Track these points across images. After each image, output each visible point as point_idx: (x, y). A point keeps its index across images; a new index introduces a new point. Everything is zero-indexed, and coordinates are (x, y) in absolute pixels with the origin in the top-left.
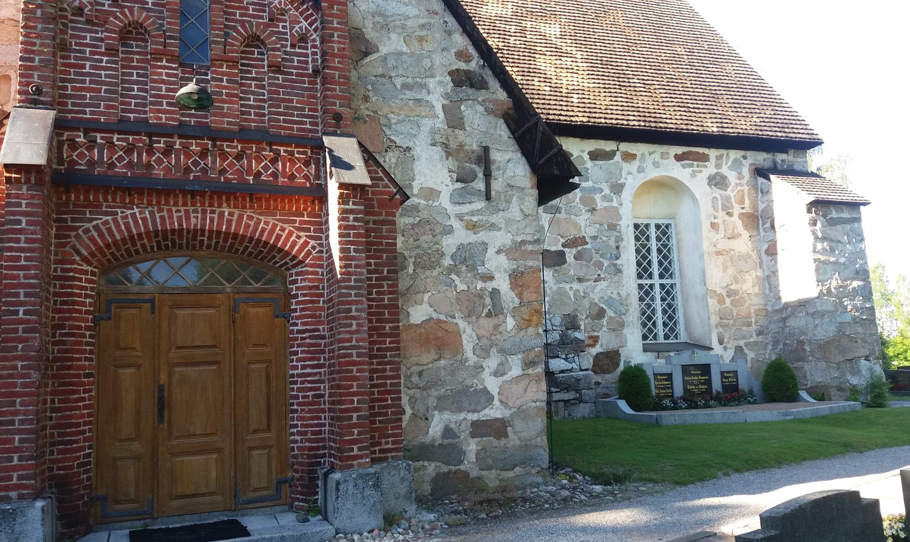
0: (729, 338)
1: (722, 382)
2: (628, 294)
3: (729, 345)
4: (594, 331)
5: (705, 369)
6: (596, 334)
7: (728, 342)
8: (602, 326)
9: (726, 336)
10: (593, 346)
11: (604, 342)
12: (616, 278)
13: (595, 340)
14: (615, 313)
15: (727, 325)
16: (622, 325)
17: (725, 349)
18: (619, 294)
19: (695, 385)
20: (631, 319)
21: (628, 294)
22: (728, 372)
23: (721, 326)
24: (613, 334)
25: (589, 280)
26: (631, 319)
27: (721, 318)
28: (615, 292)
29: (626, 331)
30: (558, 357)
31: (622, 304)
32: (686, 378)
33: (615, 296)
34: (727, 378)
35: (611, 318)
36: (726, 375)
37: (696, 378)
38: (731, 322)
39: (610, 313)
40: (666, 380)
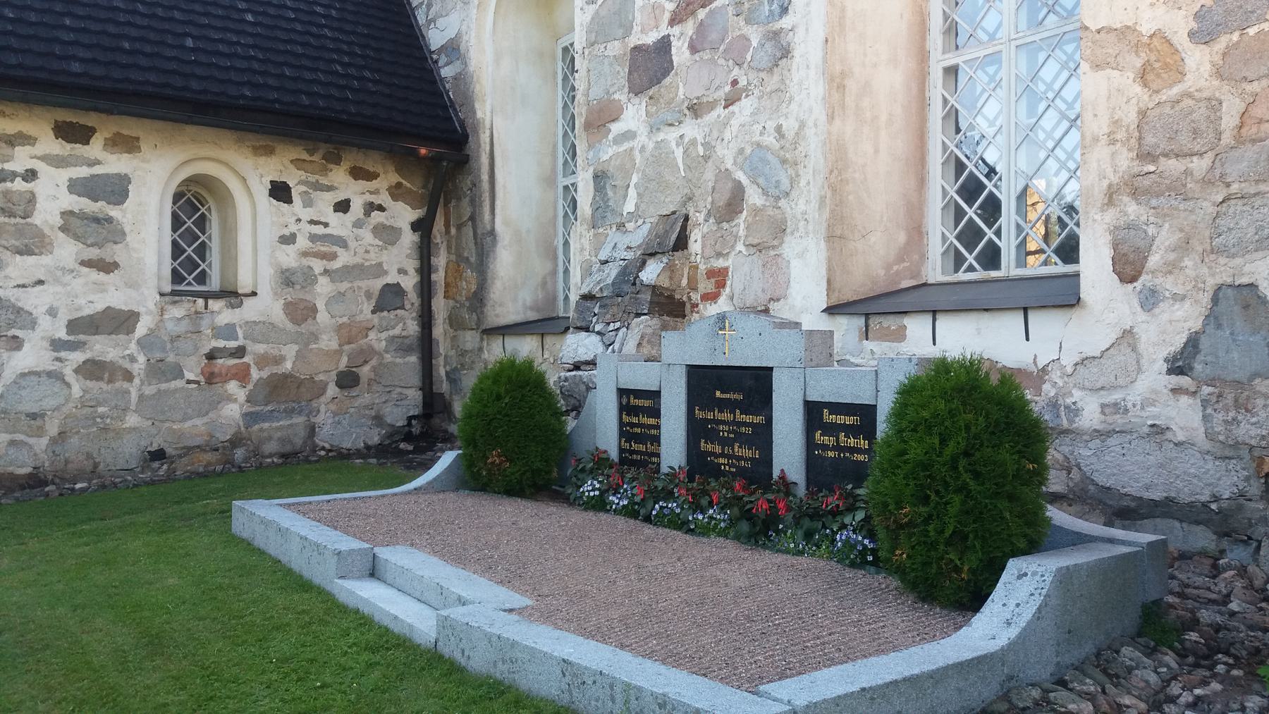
0: (1184, 246)
1: (810, 444)
2: (802, 125)
3: (1169, 284)
4: (719, 255)
5: (754, 385)
6: (720, 263)
7: (1171, 268)
8: (736, 237)
9: (1165, 237)
10: (712, 297)
11: (738, 287)
12: (773, 82)
13: (719, 277)
14: (765, 193)
15: (1177, 189)
16: (780, 230)
17: (1150, 300)
18: (779, 129)
19: (724, 442)
20: (801, 206)
21: (802, 125)
22: (836, 408)
23: (1135, 193)
24: (757, 260)
25: (712, 106)
26: (801, 206)
27: (1146, 156)
28: (771, 125)
29: (791, 247)
30: (587, 329)
31: (784, 162)
32: (699, 414)
33: (770, 140)
34: (831, 429)
35: (756, 211)
36: (828, 417)
37: (726, 416)
38: (1200, 165)
39: (754, 197)
40: (851, 430)
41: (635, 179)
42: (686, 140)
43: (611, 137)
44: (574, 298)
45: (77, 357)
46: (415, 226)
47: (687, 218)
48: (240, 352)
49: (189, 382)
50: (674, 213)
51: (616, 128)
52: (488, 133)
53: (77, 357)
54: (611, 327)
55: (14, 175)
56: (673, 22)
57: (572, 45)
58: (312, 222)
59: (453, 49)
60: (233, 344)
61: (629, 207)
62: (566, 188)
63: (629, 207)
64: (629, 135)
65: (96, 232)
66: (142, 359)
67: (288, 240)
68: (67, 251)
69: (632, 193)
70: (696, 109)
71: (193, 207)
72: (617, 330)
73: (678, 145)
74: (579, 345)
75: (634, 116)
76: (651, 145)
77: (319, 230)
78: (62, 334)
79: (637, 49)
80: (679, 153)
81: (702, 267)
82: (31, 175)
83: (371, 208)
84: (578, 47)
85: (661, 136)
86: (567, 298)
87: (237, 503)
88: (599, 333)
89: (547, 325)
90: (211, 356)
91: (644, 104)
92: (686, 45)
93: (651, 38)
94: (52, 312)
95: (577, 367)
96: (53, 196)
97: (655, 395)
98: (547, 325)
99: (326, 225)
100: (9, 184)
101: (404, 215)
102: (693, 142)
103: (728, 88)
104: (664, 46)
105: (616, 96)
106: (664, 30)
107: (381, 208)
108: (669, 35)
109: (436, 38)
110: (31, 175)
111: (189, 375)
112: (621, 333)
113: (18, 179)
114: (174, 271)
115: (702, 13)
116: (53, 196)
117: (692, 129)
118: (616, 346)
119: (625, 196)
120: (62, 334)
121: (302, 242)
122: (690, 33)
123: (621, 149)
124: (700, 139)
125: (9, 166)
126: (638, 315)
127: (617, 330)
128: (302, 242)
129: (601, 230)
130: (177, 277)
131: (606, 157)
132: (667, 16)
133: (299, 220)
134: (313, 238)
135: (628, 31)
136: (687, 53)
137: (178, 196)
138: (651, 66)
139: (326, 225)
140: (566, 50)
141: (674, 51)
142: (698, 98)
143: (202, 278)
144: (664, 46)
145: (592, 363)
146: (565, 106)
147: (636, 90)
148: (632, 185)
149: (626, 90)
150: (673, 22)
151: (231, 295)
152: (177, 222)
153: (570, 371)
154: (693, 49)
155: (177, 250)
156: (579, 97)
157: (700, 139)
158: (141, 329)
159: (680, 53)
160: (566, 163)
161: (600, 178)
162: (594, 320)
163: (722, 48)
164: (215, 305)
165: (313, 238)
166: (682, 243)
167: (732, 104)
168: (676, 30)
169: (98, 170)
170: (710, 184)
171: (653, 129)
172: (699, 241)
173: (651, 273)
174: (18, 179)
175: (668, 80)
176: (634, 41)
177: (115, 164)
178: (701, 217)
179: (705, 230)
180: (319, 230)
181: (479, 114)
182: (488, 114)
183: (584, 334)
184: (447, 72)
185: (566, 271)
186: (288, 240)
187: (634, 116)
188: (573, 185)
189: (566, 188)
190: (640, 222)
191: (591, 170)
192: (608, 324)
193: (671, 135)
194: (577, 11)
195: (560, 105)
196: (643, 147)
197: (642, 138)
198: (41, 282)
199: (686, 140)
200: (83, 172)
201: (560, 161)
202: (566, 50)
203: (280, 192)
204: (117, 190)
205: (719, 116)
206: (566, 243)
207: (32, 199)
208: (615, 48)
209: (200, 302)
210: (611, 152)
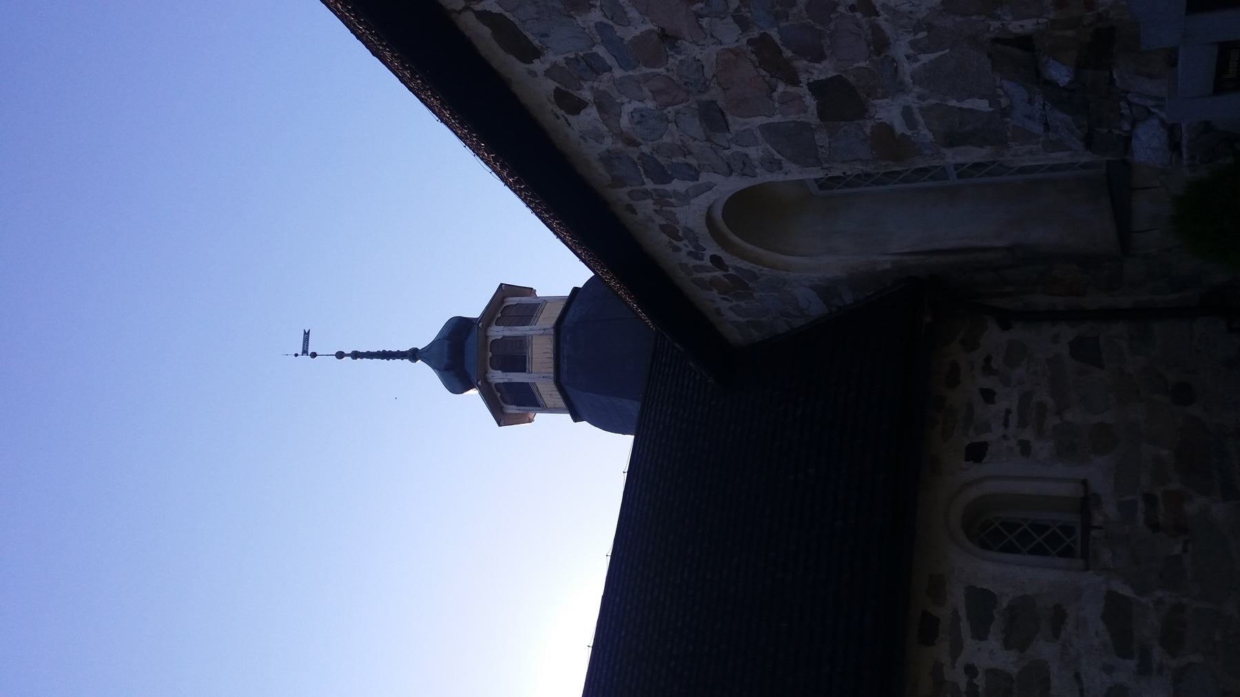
25: (876, 28)
41: (953, 103)
42: (911, 52)
43: (909, 133)
44: (1087, 157)
45: (1158, 653)
46: (1005, 326)
47: (996, 40)
48: (1150, 499)
49: (1185, 550)
50: (990, 56)
51: (900, 127)
52: (905, 258)
53: (1158, 653)
54: (1126, 111)
55: (971, 684)
56: (796, 83)
57: (816, 180)
58: (1006, 424)
59: (826, 291)
60: (1141, 505)
61: (983, 105)
62: (960, 176)
63: (983, 105)
64: (907, 113)
65: (1022, 622)
66: (1159, 594)
67: (1025, 448)
68: (1044, 649)
69: (967, 104)
70: (880, 44)
71: (997, 531)
72: (1130, 104)
73: (917, 60)
74: (1148, 144)
75: (888, 112)
76: (917, 89)
77: (1014, 419)
78: (1132, 664)
79: (822, 115)
80: (925, 58)
81: (1052, 15)
82: (970, 670)
83: (987, 369)
84: (819, 174)
85: (908, 80)
86: (1085, 166)
87: (632, 437)
88: (1133, 125)
89: (1118, 185)
90: (1155, 527)
91: (876, 102)
92: (817, 65)
93: (811, 102)
94: (1109, 669)
95: (1175, 147)
96: (990, 653)
97: (1225, 48)
98: (1118, 185)
99: (1008, 412)
100: (980, 690)
101: (994, 338)
102: (913, 44)
103: (858, 15)
104: (817, 88)
105: (868, 131)
106: (804, 90)
107: (988, 359)
108: (809, 84)
109: (817, 308)
110: (970, 670)
111: (1177, 549)
112: (1135, 100)
113: (975, 681)
114: (1031, 552)
115: (787, 53)
116: (990, 653)
117: (901, 49)
118: (1150, 103)
119: (971, 111)
120: (1132, 664)
121: (1028, 435)
122: (805, 62)
123: (921, 120)
124: (911, 37)
125: (963, 685)
126: (1112, 81)
127: (1130, 104)
128: (1028, 435)
129: (1009, 134)
130: (1067, 553)
131: (930, 136)
132: (791, 89)
133: (1004, 437)
134: (1022, 424)
135: (803, 127)
136: (825, 63)
137: (984, 545)
138: (840, 100)
139: (1008, 412)
140: (821, 187)
141: (823, 77)
142: (868, 45)
143: (1068, 530)
144: (817, 88)
145: (1172, 130)
146: (876, 183)
147: (862, 111)
148: (959, 105)
149: (862, 122)
150: (796, 83)
151: (1086, 503)
152: (1009, 549)
153: (1180, 155)
154: (819, 57)
155: (1038, 551)
156: (869, 169)
157: (911, 37)
158: (1126, 591)
159: (824, 71)
160: (933, 178)
161: (952, 140)
162: (1117, 132)
163: (819, 27)
164: (1098, 519)
165: (1022, 424)
166: (1025, 42)
167: (874, 7)
168: (803, 77)
169: (962, 613)
170: (958, 19)
171: (901, 89)
172: (1020, 23)
173: (1060, 74)
174: (975, 681)
175: (852, 80)
176: (812, 117)
177: (957, 597)
178: (995, 24)
179: (1009, 18)
180: (1014, 419)
181: (888, 266)
182: (887, 258)
183: (1134, 142)
184: (848, 299)
185: (1053, 168)
186: (1025, 448)
187: (888, 112)
188: (956, 169)
189: (960, 176)
190: (1000, 92)
191: (944, 150)
192: (1122, 116)
193: (907, 68)
194: (789, 178)
195: (874, 188)
196: (919, 97)
197: (910, 99)
198: (1077, 676)
199: (911, 52)
200: (965, 626)
201: (931, 184)
202: (821, 187)
203: (977, 453)
204: (981, 602)
205: (886, 20)
206: (1022, 170)
207: (992, 673)
208: (821, 138)
209: (1094, 533)
210: (925, 131)
